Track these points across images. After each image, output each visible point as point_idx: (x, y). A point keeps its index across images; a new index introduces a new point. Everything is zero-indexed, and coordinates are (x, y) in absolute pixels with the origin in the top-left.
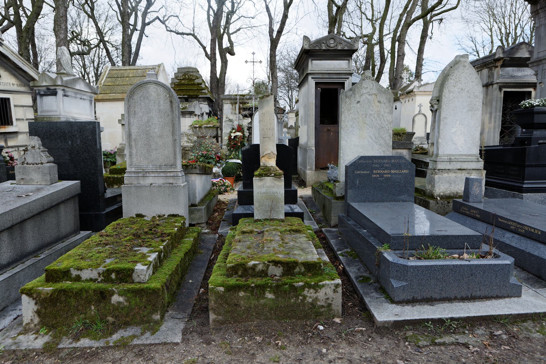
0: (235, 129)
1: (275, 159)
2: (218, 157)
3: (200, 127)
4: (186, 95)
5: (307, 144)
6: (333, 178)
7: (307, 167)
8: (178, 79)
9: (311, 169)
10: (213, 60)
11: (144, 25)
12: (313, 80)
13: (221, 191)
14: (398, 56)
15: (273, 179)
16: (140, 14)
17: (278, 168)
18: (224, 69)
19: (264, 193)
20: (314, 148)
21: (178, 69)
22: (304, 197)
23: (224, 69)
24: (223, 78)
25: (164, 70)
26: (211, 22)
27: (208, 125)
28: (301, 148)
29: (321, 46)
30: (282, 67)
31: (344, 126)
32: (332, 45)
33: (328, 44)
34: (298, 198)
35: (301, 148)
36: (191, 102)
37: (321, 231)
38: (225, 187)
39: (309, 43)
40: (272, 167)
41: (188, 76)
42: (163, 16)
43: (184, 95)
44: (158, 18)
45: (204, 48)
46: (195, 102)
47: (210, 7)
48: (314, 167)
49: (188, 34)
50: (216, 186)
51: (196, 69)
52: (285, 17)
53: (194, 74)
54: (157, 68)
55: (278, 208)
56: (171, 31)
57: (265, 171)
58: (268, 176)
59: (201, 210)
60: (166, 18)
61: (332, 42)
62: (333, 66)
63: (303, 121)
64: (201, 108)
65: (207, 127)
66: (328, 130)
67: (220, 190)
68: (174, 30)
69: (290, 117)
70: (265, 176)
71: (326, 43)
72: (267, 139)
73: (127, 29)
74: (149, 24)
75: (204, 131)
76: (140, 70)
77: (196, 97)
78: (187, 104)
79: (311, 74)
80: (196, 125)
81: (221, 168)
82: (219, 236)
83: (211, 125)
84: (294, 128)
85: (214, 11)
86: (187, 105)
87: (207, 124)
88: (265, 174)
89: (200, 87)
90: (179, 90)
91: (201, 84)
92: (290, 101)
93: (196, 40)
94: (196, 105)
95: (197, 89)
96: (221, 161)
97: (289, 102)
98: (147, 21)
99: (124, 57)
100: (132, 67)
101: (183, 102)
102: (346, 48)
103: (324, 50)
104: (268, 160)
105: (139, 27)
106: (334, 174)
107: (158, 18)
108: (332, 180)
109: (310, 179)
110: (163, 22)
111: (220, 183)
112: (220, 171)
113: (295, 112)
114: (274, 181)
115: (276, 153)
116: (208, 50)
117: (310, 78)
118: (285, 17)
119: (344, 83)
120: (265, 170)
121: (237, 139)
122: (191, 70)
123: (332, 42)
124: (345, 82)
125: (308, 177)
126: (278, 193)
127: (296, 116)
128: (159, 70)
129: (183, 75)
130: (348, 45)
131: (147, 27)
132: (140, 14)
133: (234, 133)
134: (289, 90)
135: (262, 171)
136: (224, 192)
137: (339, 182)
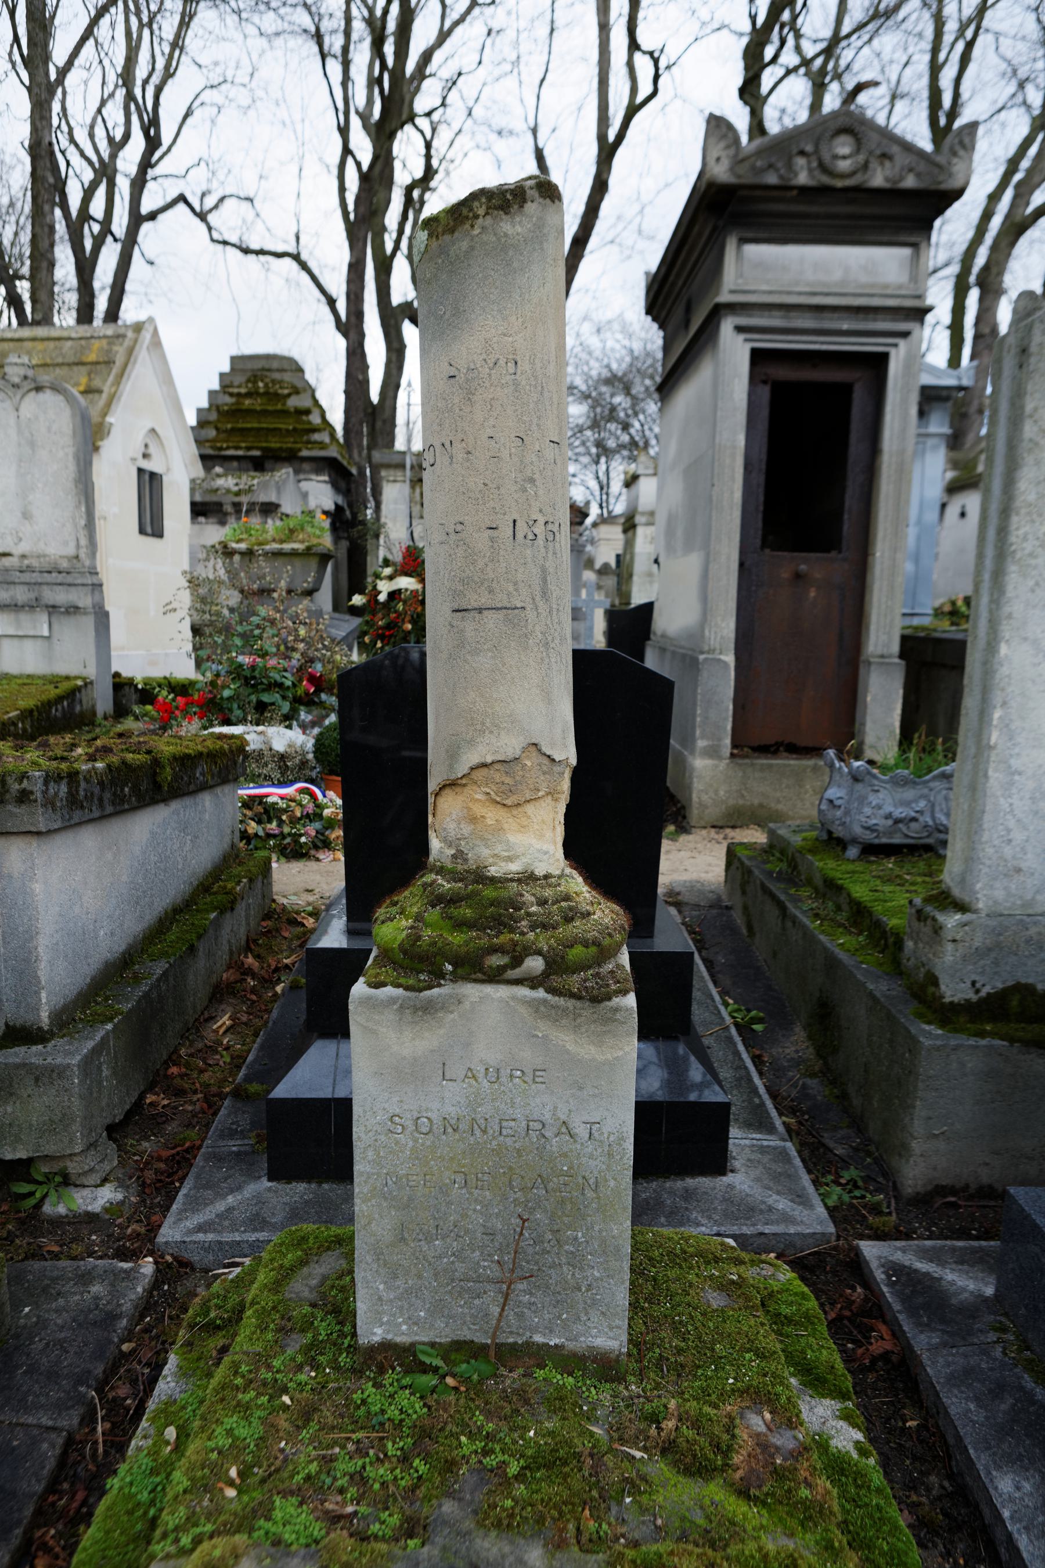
0: (394, 564)
1: (562, 809)
2: (313, 679)
3: (249, 554)
4: (257, 448)
5: (696, 635)
6: (858, 830)
7: (694, 741)
8: (231, 395)
9: (712, 752)
10: (352, 335)
11: (137, 219)
12: (741, 337)
13: (301, 846)
14: (977, 337)
15: (535, 1005)
16: (123, 185)
17: (577, 884)
18: (394, 372)
19: (451, 1126)
20: (730, 659)
21: (234, 360)
22: (685, 898)
23: (394, 372)
24: (388, 403)
25: (156, 343)
26: (351, 207)
27: (287, 547)
28: (663, 650)
29: (789, 166)
30: (579, 382)
31: (1029, 546)
32: (844, 165)
33: (827, 158)
34: (660, 905)
35: (663, 650)
36: (272, 470)
37: (857, 1266)
38: (318, 825)
39: (732, 151)
40: (529, 878)
41: (266, 385)
42: (199, 194)
43: (248, 449)
44: (182, 198)
45: (331, 302)
46: (285, 473)
47: (347, 151)
48: (728, 741)
49: (279, 255)
50: (281, 823)
51: (291, 361)
52: (600, 187)
53: (287, 377)
54: (130, 334)
55: (576, 1261)
56: (225, 243)
57: (460, 925)
58: (495, 977)
59: (60, 1072)
60: (210, 202)
61: (843, 147)
62: (837, 275)
63: (679, 533)
64: (305, 496)
65: (278, 554)
66: (798, 576)
67: (296, 842)
68: (234, 239)
69: (602, 536)
70: (456, 978)
71: (817, 151)
72: (491, 619)
73: (47, 208)
74: (152, 216)
75: (263, 566)
76: (69, 344)
77: (290, 457)
78: (253, 478)
79: (732, 308)
80: (239, 541)
81: (316, 731)
82: (163, 1272)
83: (296, 546)
84: (613, 572)
85: (358, 164)
86: (255, 482)
87: (282, 542)
88: (458, 962)
89: (304, 422)
90: (233, 430)
91: (308, 412)
92: (602, 488)
93: (305, 277)
94: (285, 481)
95: (295, 430)
96: (323, 696)
97: (597, 493)
98: (147, 206)
99: (38, 306)
100: (41, 331)
101: (247, 470)
102: (910, 182)
103: (803, 190)
104: (491, 815)
105: (120, 224)
106: (867, 811)
107: (182, 198)
108: (854, 841)
109: (705, 798)
110: (202, 216)
111: (300, 805)
112: (310, 744)
113: (622, 520)
114: (543, 1028)
115: (568, 753)
116: (342, 306)
117: (727, 326)
118: (600, 187)
119: (882, 359)
120: (466, 912)
121: (400, 607)
122: (275, 365)
123: (845, 150)
124: (893, 352)
125: (697, 786)
126: (582, 1131)
127: (625, 531)
128: (136, 341)
129: (248, 381)
130: (922, 167)
131: (146, 227)
132: (123, 185)
133: (391, 578)
134: (598, 456)
135: (433, 914)
136: (316, 847)
137: (962, 907)
